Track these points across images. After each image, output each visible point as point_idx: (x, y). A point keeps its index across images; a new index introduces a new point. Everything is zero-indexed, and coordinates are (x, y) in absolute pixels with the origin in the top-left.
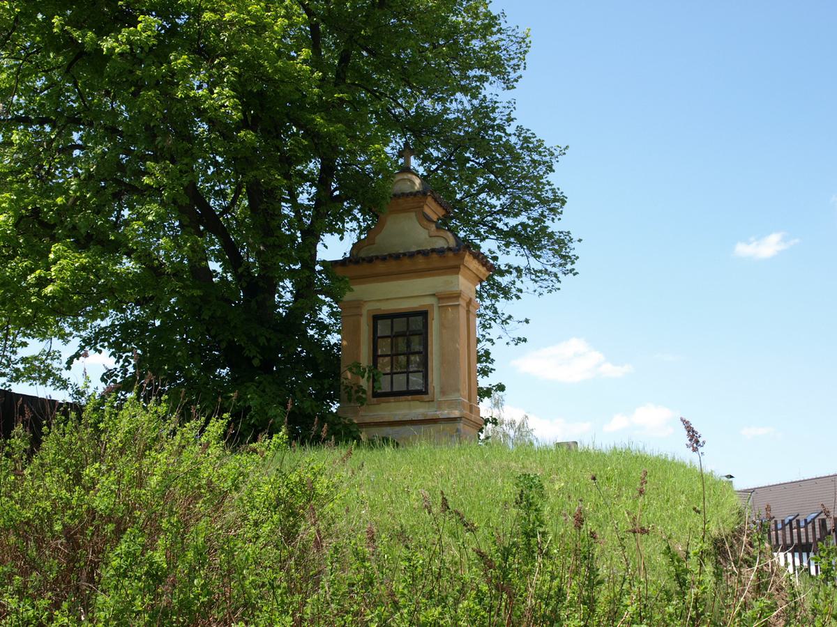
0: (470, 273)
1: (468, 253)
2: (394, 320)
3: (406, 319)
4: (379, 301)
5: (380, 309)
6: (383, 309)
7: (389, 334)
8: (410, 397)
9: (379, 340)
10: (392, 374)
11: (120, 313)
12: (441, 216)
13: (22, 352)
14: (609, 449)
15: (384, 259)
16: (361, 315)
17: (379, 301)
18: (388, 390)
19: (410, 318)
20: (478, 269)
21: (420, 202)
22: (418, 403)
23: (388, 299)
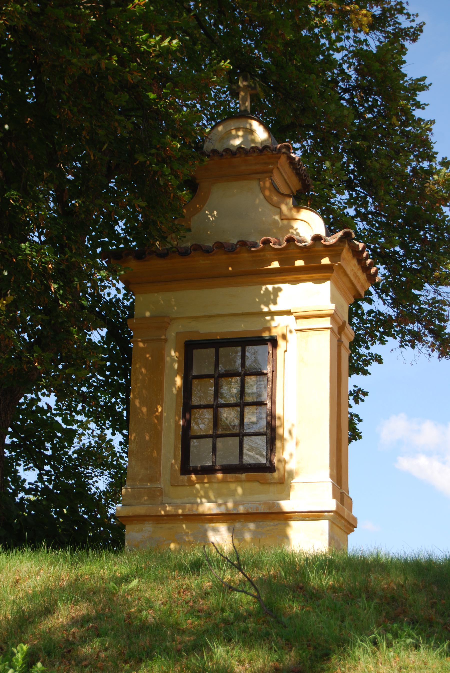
0: (345, 279)
1: (347, 246)
2: (221, 350)
3: (213, 350)
4: (196, 318)
5: (198, 332)
6: (201, 331)
7: (213, 372)
8: (244, 476)
9: (195, 382)
10: (215, 437)
11: (101, 295)
12: (295, 192)
13: (408, 328)
14: (124, 573)
15: (208, 251)
16: (166, 340)
17: (196, 318)
18: (236, 461)
19: (221, 350)
20: (356, 276)
21: (268, 164)
22: (256, 484)
23: (210, 317)
